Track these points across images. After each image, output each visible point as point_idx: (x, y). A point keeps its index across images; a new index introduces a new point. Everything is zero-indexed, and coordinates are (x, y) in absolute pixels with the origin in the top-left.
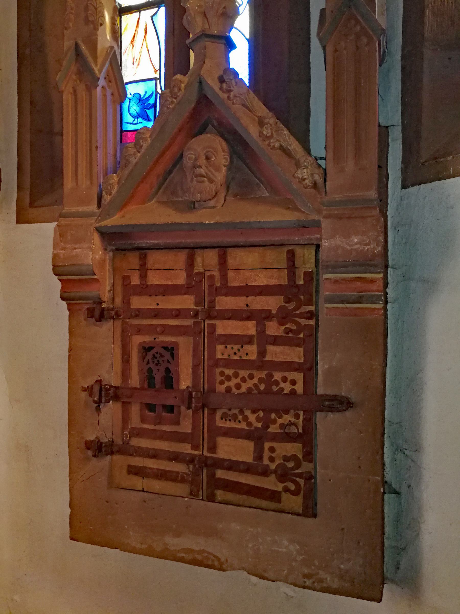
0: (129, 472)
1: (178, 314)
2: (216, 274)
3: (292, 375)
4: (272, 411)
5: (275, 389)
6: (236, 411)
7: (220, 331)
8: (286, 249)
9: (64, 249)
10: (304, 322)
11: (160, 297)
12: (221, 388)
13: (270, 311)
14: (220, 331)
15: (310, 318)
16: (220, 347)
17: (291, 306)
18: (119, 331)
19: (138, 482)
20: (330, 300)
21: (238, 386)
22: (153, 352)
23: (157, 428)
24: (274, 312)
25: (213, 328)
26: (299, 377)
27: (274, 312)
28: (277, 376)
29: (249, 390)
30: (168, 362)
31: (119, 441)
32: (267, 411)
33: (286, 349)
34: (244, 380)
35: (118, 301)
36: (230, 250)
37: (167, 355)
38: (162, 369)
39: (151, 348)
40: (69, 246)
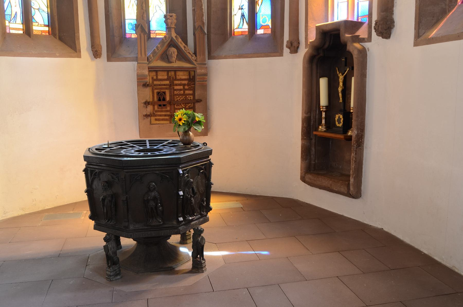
0: (155, 120)
1: (164, 85)
2: (174, 76)
3: (190, 96)
4: (186, 104)
5: (187, 99)
6: (179, 104)
7: (175, 88)
8: (188, 71)
9: (140, 71)
10: (192, 86)
11: (161, 81)
12: (176, 100)
13: (186, 84)
14: (175, 88)
15: (194, 85)
16: (175, 92)
17: (190, 83)
18: (151, 89)
19: (158, 122)
20: (198, 81)
21: (179, 99)
22: (160, 93)
23: (162, 110)
24: (186, 84)
25: (173, 88)
26: (192, 97)
27: (186, 84)
28: (187, 97)
29: (182, 100)
30: (164, 95)
31: (152, 114)
32: (186, 104)
33: (189, 91)
34: (181, 98)
35: (151, 82)
36: (176, 71)
37: (164, 94)
38: (163, 97)
39: (159, 93)
40: (141, 70)
